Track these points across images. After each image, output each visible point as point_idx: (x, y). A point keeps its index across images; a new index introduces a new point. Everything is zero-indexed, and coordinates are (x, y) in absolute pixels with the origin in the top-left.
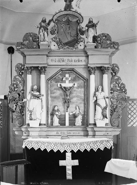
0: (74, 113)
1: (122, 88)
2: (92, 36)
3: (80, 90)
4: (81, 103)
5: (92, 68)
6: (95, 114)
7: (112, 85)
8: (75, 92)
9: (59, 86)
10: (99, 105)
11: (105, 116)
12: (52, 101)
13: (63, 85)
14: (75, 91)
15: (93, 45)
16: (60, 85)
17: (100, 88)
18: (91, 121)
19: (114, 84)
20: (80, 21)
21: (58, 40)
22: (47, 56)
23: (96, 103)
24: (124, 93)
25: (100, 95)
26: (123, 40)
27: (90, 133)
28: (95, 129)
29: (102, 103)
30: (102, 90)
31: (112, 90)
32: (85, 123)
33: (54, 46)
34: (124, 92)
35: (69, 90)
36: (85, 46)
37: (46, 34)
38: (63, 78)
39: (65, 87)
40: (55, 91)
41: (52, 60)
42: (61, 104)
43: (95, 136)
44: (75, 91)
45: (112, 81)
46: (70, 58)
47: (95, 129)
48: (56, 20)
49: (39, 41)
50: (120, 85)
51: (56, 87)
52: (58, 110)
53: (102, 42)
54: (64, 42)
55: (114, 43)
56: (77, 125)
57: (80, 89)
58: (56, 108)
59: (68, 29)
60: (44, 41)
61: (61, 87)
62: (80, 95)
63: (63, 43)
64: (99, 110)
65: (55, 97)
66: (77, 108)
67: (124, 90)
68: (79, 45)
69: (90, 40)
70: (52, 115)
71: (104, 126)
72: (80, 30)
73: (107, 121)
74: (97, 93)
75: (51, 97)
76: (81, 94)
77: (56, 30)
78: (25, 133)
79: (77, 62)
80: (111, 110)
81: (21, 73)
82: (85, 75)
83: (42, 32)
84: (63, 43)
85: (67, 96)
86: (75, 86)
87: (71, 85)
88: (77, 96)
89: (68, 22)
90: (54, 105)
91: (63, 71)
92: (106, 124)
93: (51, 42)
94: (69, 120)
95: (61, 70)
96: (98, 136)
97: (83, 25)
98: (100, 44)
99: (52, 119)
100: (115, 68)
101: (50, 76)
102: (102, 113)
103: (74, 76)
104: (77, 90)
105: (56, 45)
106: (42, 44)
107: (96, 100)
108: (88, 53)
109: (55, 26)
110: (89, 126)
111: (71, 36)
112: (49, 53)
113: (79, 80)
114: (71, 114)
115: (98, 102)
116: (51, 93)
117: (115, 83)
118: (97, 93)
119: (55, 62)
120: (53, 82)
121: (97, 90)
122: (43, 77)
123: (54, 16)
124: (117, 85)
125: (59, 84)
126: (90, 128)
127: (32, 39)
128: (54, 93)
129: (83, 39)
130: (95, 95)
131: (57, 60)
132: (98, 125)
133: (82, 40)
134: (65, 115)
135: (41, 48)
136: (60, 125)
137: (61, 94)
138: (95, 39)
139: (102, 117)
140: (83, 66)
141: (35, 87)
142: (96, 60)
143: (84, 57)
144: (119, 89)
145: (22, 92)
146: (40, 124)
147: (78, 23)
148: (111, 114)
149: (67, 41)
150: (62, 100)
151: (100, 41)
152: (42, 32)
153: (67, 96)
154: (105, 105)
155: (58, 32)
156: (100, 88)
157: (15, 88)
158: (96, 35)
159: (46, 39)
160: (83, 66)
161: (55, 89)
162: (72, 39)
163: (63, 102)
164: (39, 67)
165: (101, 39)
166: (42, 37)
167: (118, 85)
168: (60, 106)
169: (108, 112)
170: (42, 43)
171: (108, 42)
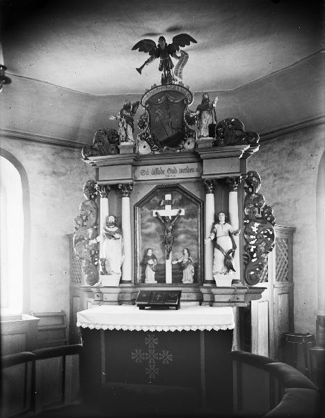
0: (180, 261)
1: (266, 215)
2: (11, 78)
3: (191, 222)
4: (192, 244)
5: (207, 181)
6: (214, 257)
7: (246, 211)
8: (182, 225)
9: (154, 215)
10: (219, 248)
11: (229, 267)
12: (144, 241)
13: (162, 213)
14: (181, 222)
15: (210, 140)
16: (157, 213)
17: (222, 217)
18: (208, 277)
19: (250, 209)
20: (187, 101)
21: (150, 136)
22: (133, 165)
23: (215, 244)
24: (268, 223)
25: (222, 229)
26: (14, 355)
27: (207, 298)
28: (213, 290)
29: (226, 243)
30: (228, 220)
31: (247, 220)
32: (199, 279)
33: (144, 149)
34: (270, 221)
35: (171, 221)
36: (196, 145)
37: (129, 129)
38: (160, 202)
39: (163, 217)
40: (149, 223)
41: (143, 172)
42: (159, 246)
43: (214, 304)
44: (181, 222)
45: (244, 203)
46: (171, 166)
47: (213, 290)
48: (146, 104)
49: (118, 140)
50: (261, 210)
51: (149, 217)
52: (153, 257)
53: (227, 135)
54: (161, 139)
55: (247, 134)
56: (185, 282)
57: (190, 220)
58: (150, 253)
59: (167, 117)
60: (126, 140)
61: (157, 218)
62: (190, 229)
63: (160, 142)
64: (220, 256)
65: (149, 235)
66: (186, 252)
67: (269, 219)
68: (186, 144)
69: (204, 132)
70: (144, 265)
71: (230, 286)
72: (187, 117)
73: (237, 275)
74: (216, 226)
75: (142, 234)
76: (192, 228)
77: (146, 119)
78: (98, 296)
79: (180, 172)
80: (246, 255)
81: (93, 197)
82: (197, 195)
83: (123, 125)
84: (160, 142)
85: (167, 232)
86: (181, 214)
87: (175, 212)
88: (186, 232)
89: (167, 104)
90: (147, 248)
91: (162, 189)
92: (234, 281)
93: (138, 142)
94: (173, 274)
95: (157, 188)
96: (219, 304)
97: (193, 106)
98: (223, 137)
99: (144, 272)
100: (252, 180)
101: (140, 198)
102: (225, 261)
103: (181, 197)
104: (185, 220)
105: (148, 146)
106: (123, 146)
107: (215, 239)
108: (201, 156)
109: (145, 114)
110: (205, 285)
111: (172, 128)
112: (137, 161)
113: (188, 204)
114: (175, 262)
115: (219, 242)
116: (142, 228)
117: (252, 206)
118: (216, 226)
119: (151, 175)
120: (146, 210)
121: (217, 221)
122: (126, 201)
123: (143, 97)
124: (256, 209)
125: (154, 211)
126: (206, 287)
127: (108, 139)
128: (147, 227)
129: (194, 131)
130: (213, 228)
131: (150, 171)
132: (218, 284)
133: (191, 134)
134: (165, 264)
135: (121, 152)
136: (156, 282)
137: (157, 230)
138: (212, 130)
139: (225, 270)
140: (195, 179)
141: (112, 219)
142: (215, 169)
143: (196, 164)
144: (260, 216)
145: (95, 227)
146: (121, 281)
147: (184, 105)
148: (245, 263)
149: (166, 137)
150: (159, 238)
151: (223, 132)
152: (123, 125)
153: (167, 232)
154: (231, 247)
155: (150, 123)
156: (222, 217)
157: (83, 221)
158: (215, 123)
159: (131, 137)
160: (195, 179)
161: (149, 221)
162: (174, 133)
163: (161, 242)
164: (118, 184)
165: (224, 129)
166: (123, 133)
167: (259, 210)
168: (156, 249)
169: (236, 262)
170: (123, 144)
171: (238, 133)
